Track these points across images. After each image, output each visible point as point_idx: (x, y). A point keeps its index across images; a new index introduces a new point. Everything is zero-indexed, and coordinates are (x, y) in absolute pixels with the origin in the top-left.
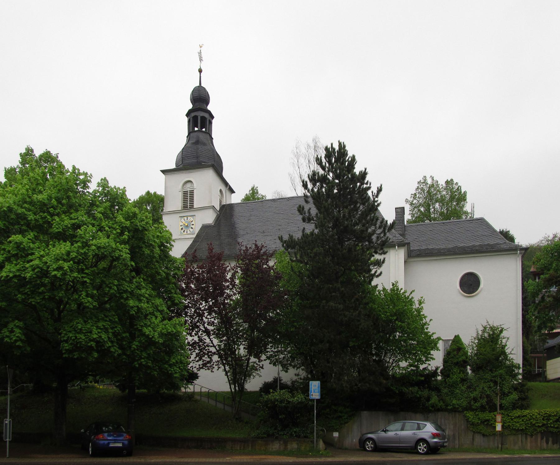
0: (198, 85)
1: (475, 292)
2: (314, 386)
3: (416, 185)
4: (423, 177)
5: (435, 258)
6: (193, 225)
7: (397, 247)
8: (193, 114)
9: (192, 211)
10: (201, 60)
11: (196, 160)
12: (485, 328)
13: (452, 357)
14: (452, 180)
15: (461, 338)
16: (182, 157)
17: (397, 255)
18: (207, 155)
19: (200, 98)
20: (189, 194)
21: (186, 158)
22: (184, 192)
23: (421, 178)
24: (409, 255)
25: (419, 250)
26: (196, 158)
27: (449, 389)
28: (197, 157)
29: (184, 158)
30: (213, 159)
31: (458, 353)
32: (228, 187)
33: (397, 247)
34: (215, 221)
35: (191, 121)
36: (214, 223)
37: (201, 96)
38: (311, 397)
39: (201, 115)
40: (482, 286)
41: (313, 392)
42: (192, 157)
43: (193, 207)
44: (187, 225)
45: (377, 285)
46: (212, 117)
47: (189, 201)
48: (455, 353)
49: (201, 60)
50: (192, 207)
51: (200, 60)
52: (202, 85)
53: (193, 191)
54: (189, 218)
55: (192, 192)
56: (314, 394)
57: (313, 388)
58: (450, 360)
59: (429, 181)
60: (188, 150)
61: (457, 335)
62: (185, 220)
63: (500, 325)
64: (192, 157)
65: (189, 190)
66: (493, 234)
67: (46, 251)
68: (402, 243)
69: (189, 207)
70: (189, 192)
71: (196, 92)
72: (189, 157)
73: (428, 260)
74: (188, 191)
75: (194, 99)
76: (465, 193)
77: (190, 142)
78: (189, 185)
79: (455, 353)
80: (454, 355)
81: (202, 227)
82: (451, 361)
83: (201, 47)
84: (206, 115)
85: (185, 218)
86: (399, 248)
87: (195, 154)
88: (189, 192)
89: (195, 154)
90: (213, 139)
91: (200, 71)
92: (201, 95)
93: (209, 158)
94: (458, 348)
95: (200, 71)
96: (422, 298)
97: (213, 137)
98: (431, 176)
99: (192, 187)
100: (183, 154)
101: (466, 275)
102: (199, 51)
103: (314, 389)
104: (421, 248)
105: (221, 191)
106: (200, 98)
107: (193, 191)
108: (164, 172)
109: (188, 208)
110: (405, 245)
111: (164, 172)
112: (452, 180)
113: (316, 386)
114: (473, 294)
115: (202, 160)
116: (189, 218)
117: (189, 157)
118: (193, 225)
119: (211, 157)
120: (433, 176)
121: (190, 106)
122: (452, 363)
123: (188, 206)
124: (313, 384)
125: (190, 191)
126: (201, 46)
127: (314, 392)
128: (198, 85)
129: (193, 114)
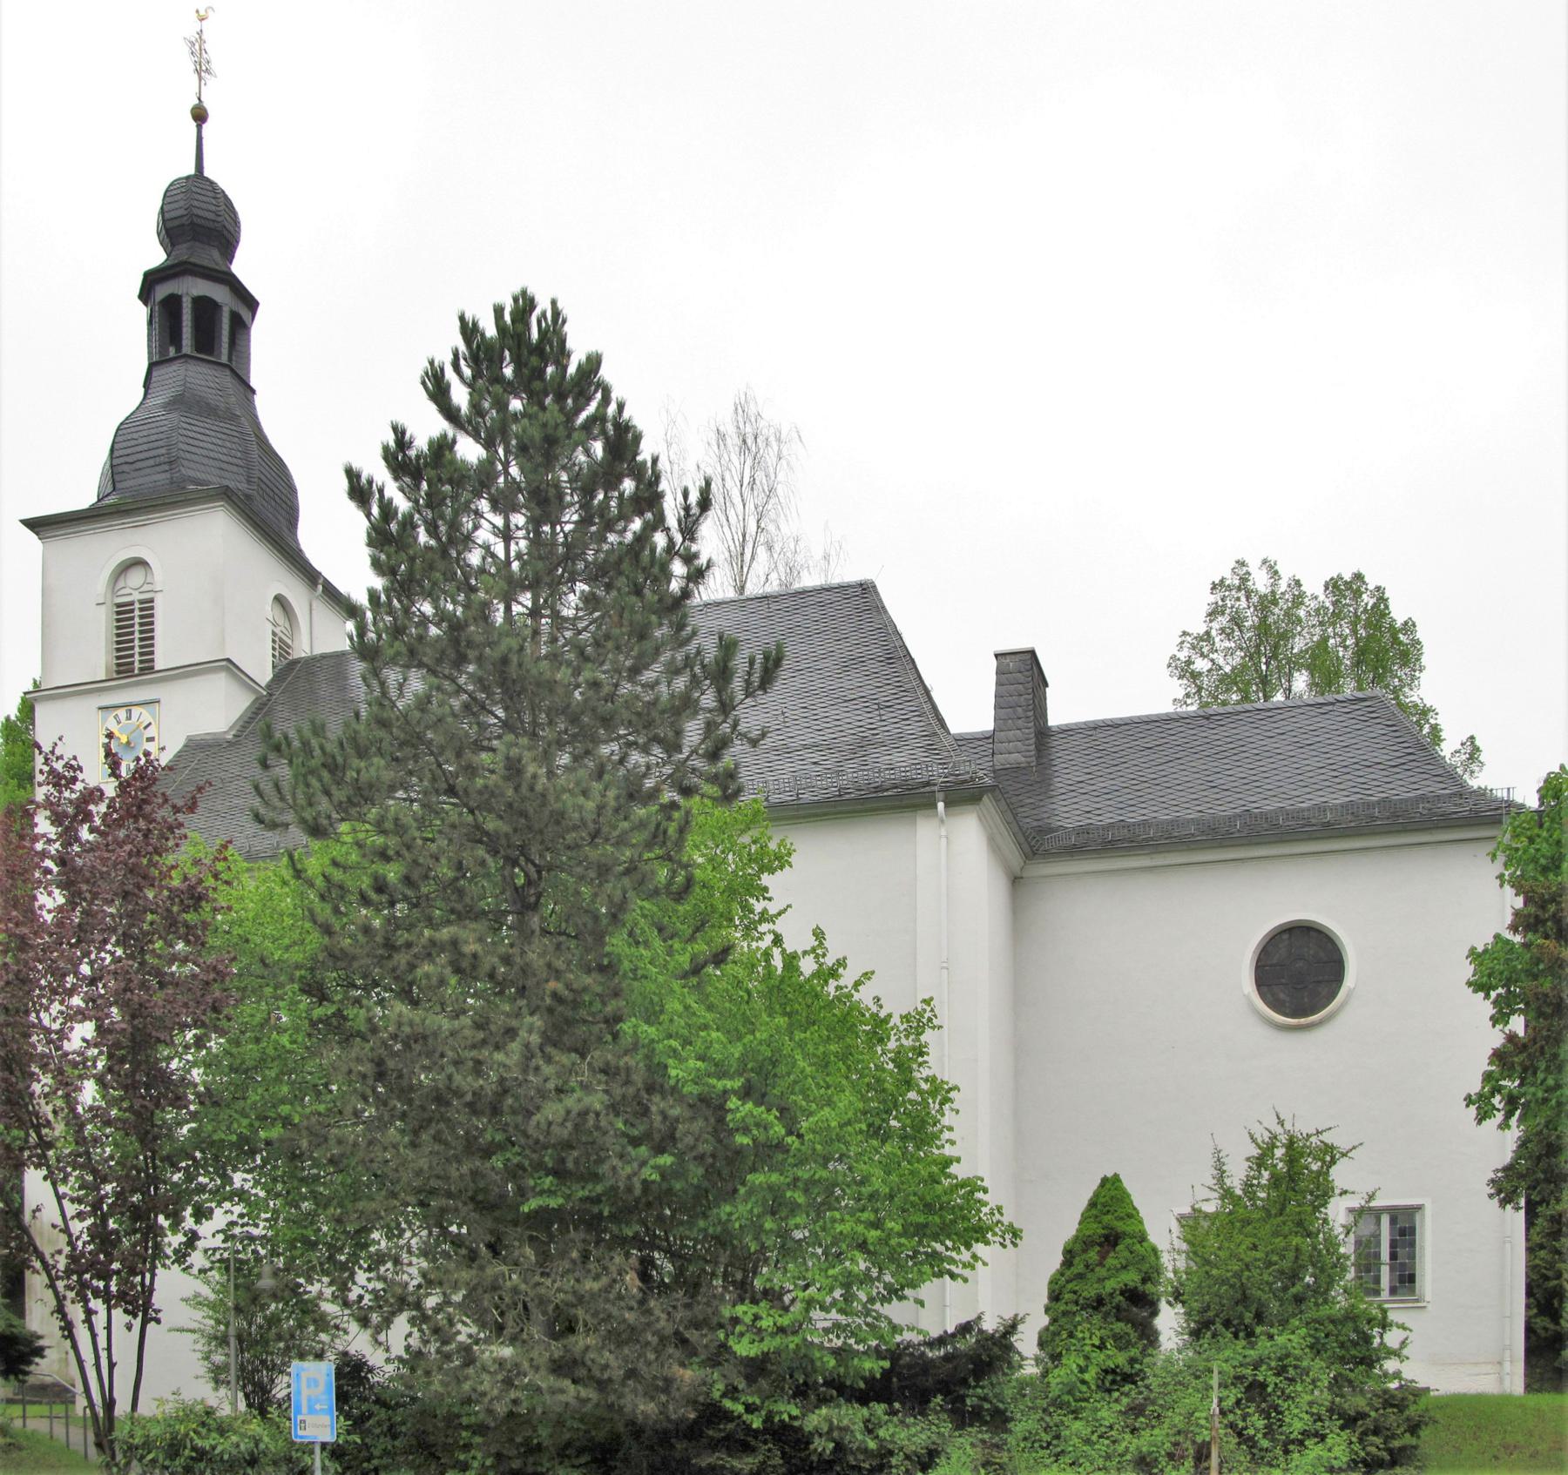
0: (191, 170)
1: (1324, 1007)
2: (309, 1386)
3: (1207, 599)
4: (1233, 564)
5: (1145, 861)
6: (151, 739)
7: (941, 805)
8: (162, 292)
9: (151, 682)
10: (202, 70)
11: (168, 475)
12: (1267, 1150)
13: (1080, 1276)
14: (1359, 577)
15: (1130, 1190)
16: (112, 466)
17: (944, 841)
18: (216, 455)
19: (192, 223)
20: (137, 613)
21: (126, 468)
22: (118, 605)
23: (1224, 571)
24: (1027, 849)
25: (1083, 831)
26: (166, 467)
27: (1048, 1419)
28: (170, 463)
29: (120, 469)
30: (241, 470)
31: (1103, 1257)
32: (320, 588)
33: (941, 805)
34: (241, 723)
35: (156, 320)
36: (233, 732)
37: (197, 216)
38: (302, 1435)
39: (196, 292)
40: (1349, 981)
41: (304, 1410)
42: (151, 462)
43: (153, 668)
44: (128, 743)
45: (1480, 1122)
46: (252, 304)
47: (137, 643)
48: (1093, 1255)
49: (202, 70)
50: (148, 667)
51: (198, 72)
52: (206, 174)
53: (152, 601)
54: (136, 711)
55: (148, 606)
56: (309, 1419)
57: (305, 1392)
58: (1070, 1286)
59: (1261, 582)
60: (135, 436)
61: (1109, 1175)
62: (119, 722)
63: (1318, 1133)
64: (151, 462)
65: (136, 596)
66: (1411, 757)
67: (356, 1016)
68: (965, 786)
69: (141, 669)
70: (137, 606)
71: (176, 198)
72: (139, 465)
73: (1118, 870)
74: (132, 603)
75: (167, 231)
76: (1409, 626)
77: (150, 402)
78: (135, 578)
79: (1093, 1255)
80: (1087, 1266)
81: (185, 746)
82: (1075, 1292)
83: (202, 20)
84: (219, 293)
85: (122, 713)
86: (957, 809)
87: (163, 451)
88: (137, 606)
89: (163, 451)
90: (253, 392)
91: (200, 116)
92: (196, 211)
93: (225, 466)
94: (1107, 1237)
95: (200, 116)
96: (927, 1002)
97: (253, 383)
98: (1265, 562)
99: (146, 588)
100: (116, 454)
101: (1285, 936)
102: (193, 36)
103: (309, 1400)
104: (1095, 820)
105: (280, 600)
106: (192, 223)
107: (152, 601)
108: (37, 525)
109: (136, 672)
110: (980, 799)
111: (37, 525)
112: (1359, 577)
113: (316, 1382)
114: (1303, 1021)
115: (191, 473)
116: (136, 711)
117: (139, 465)
118: (151, 739)
119: (235, 461)
120: (1272, 558)
121: (157, 256)
122: (1076, 1303)
123: (137, 665)
124: (304, 1376)
125: (141, 602)
126: (202, 13)
127: (312, 1411)
128: (191, 170)
129: (162, 292)
